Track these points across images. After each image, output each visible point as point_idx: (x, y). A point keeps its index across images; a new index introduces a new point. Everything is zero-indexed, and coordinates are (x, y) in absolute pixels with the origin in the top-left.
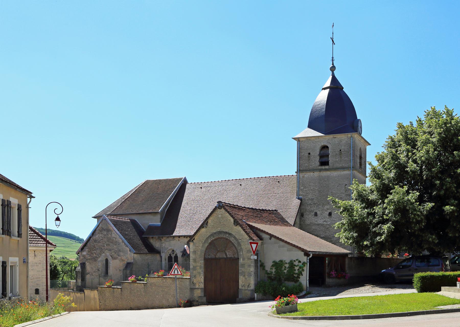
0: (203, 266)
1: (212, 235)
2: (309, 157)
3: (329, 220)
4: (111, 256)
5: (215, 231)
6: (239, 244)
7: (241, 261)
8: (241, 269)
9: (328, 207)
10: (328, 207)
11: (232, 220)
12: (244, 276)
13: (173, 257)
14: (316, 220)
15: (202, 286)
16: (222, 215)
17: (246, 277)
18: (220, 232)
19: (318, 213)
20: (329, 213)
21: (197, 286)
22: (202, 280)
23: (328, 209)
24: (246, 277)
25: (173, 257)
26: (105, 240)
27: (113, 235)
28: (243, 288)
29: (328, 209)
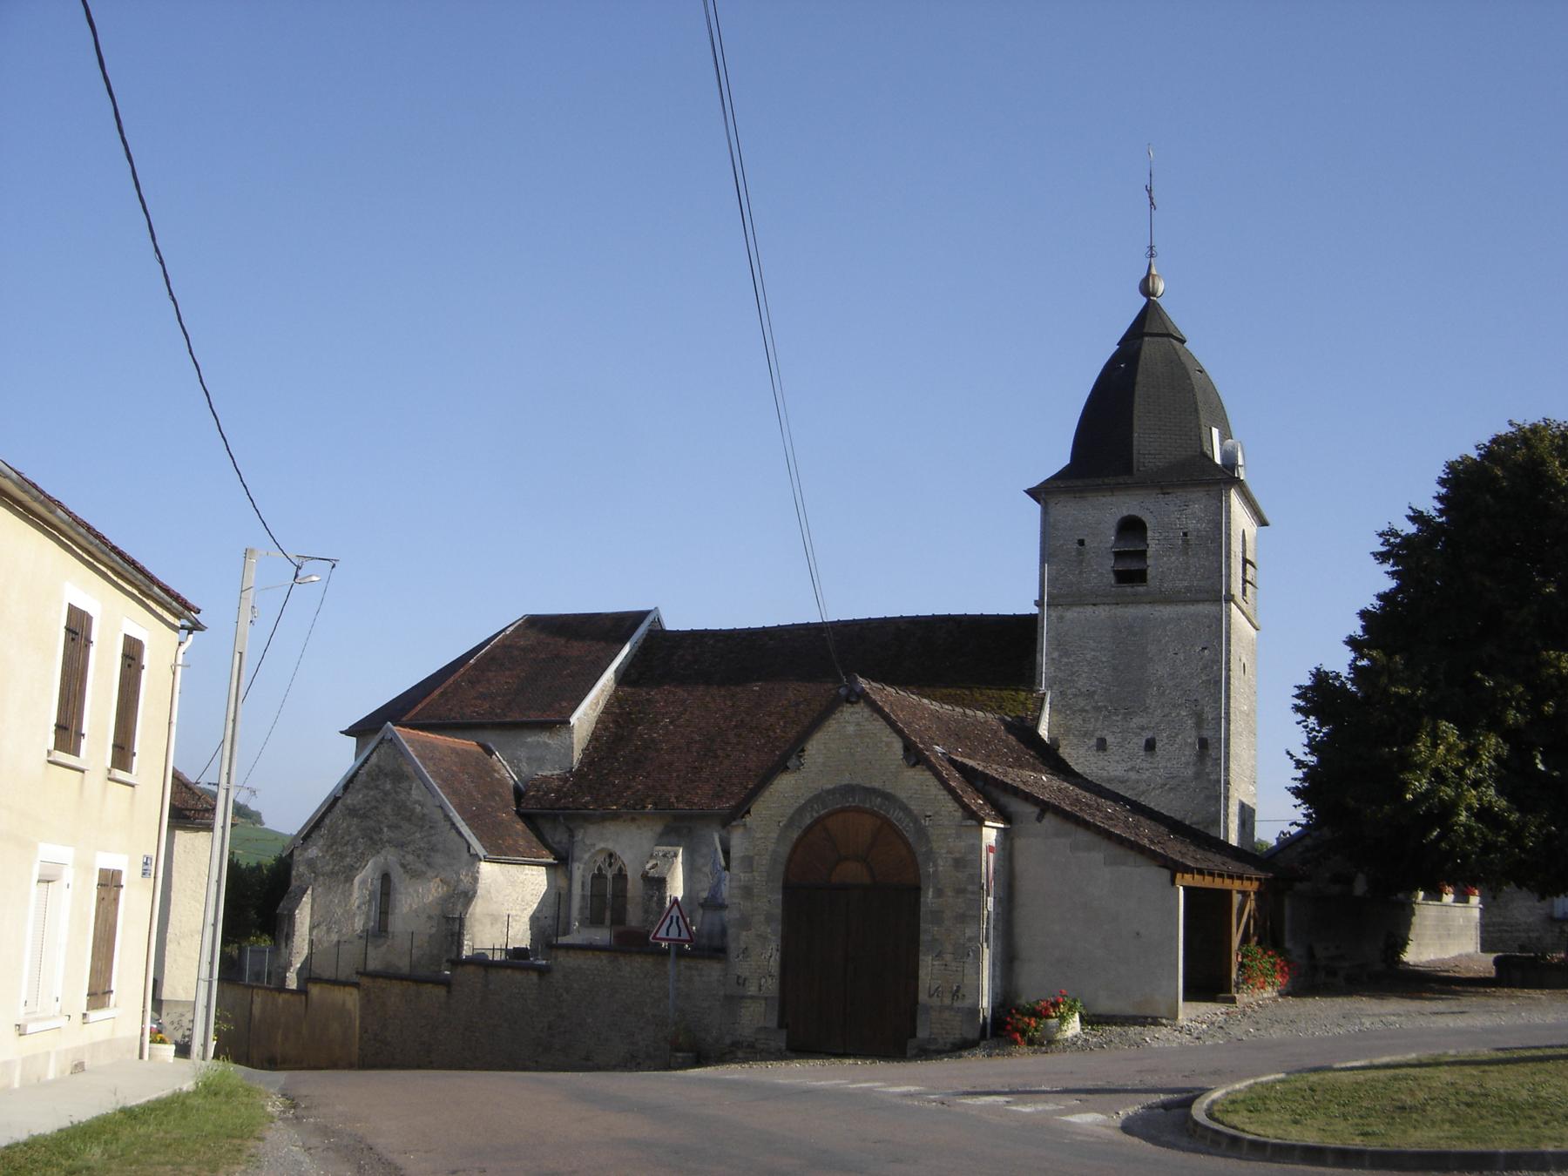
0: (778, 911)
1: (819, 798)
2: (1080, 553)
3: (1145, 765)
4: (403, 866)
5: (830, 786)
6: (922, 832)
7: (929, 897)
8: (928, 931)
9: (1143, 721)
10: (1143, 721)
11: (898, 745)
12: (939, 955)
13: (610, 876)
14: (1101, 764)
15: (772, 986)
16: (858, 724)
17: (948, 957)
18: (849, 790)
19: (1110, 739)
20: (1148, 741)
21: (752, 990)
22: (774, 965)
23: (1143, 728)
24: (948, 957)
25: (610, 876)
26: (388, 809)
27: (416, 794)
28: (935, 1001)
29: (1143, 728)
